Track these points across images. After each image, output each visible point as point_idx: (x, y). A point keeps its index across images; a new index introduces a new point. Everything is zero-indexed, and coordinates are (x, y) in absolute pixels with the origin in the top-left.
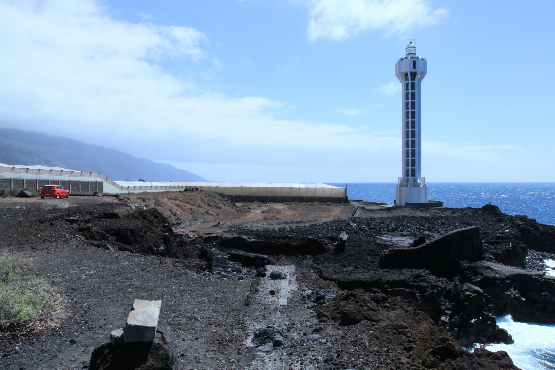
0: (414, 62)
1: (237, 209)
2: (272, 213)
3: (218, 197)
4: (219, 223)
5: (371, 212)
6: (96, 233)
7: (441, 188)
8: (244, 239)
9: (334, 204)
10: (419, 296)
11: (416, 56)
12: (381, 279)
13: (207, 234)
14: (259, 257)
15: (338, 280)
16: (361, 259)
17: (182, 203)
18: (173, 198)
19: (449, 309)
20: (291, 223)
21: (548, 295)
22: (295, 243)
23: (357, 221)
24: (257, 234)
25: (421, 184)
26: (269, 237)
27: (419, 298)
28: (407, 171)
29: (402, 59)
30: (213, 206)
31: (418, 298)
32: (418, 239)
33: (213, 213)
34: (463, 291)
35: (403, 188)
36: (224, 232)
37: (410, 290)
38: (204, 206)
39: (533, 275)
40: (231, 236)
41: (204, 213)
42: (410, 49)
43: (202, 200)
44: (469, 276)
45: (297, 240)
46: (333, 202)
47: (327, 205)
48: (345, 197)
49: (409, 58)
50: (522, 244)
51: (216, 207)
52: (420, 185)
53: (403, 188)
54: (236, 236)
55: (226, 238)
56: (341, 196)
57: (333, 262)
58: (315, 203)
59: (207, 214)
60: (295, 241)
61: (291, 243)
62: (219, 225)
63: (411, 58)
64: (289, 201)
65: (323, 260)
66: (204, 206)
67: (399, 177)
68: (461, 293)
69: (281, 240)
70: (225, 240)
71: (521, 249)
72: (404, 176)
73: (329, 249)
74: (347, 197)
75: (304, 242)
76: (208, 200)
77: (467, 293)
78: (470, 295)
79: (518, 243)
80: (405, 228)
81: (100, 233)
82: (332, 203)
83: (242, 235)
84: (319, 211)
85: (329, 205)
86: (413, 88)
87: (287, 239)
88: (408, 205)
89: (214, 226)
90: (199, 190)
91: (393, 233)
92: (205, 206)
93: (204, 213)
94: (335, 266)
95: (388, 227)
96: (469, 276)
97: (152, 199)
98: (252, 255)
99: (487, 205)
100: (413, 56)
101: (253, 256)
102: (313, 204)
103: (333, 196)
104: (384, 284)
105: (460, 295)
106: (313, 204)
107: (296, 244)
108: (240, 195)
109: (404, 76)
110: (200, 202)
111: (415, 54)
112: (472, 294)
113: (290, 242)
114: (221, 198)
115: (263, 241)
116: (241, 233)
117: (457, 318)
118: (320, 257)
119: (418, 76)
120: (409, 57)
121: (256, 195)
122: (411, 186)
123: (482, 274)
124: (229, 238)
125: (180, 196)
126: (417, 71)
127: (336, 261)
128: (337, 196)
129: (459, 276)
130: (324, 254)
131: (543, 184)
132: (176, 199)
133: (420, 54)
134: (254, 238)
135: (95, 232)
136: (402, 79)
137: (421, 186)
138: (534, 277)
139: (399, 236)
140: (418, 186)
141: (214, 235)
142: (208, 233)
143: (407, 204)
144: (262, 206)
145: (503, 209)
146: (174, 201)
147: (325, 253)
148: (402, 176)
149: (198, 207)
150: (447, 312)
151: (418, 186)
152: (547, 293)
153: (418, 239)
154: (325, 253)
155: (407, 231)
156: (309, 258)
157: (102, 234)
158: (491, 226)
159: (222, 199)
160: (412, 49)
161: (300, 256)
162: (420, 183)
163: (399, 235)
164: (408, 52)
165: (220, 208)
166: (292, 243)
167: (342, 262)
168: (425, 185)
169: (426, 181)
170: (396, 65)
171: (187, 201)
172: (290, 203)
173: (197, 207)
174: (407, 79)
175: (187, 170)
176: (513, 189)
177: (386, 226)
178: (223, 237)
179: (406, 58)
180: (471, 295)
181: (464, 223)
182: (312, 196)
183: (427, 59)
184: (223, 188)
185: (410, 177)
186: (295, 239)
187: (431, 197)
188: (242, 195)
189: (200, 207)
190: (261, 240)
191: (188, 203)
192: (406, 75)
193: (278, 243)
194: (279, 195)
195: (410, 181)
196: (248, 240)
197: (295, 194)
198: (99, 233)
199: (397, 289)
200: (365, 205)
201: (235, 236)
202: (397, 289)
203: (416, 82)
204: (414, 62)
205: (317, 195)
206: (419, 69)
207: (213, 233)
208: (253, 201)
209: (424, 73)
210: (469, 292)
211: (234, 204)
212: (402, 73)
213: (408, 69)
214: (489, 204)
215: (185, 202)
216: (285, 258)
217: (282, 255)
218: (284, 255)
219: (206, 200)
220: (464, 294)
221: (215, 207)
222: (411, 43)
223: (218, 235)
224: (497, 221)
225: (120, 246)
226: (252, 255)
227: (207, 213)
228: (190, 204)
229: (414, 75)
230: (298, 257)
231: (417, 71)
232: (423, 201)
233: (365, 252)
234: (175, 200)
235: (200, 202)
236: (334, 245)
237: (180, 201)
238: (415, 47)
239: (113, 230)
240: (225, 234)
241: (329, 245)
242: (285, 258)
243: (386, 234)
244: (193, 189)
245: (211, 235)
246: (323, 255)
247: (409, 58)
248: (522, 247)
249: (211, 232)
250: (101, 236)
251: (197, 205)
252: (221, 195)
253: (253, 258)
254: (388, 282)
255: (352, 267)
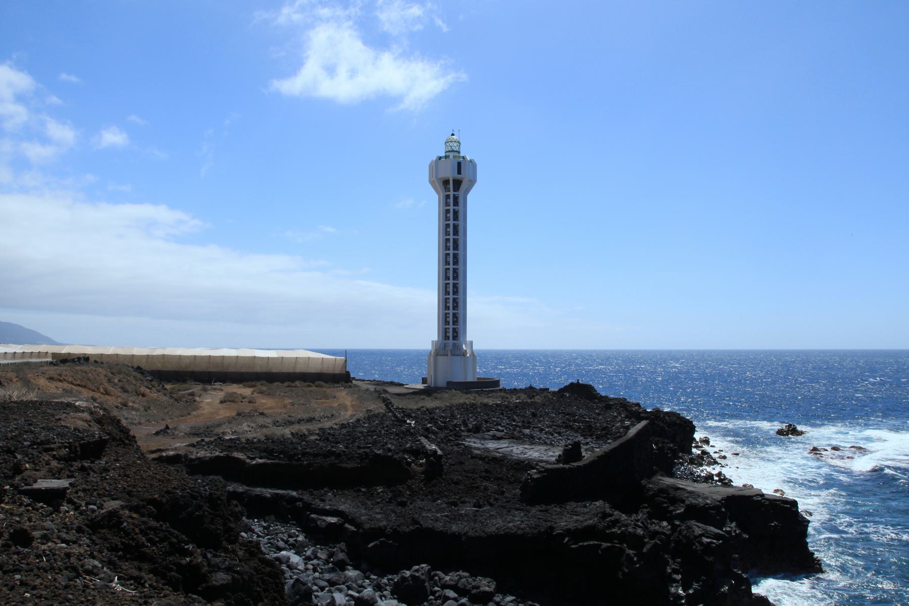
0: (459, 164)
1: (173, 397)
2: (240, 403)
3: (133, 373)
4: (167, 427)
5: (403, 397)
6: (141, 531)
7: (500, 357)
8: (238, 458)
9: (328, 385)
10: (634, 554)
11: (462, 155)
12: (552, 528)
13: (153, 452)
14: (282, 497)
15: (465, 534)
16: (477, 487)
17: (73, 386)
18: (56, 376)
19: (675, 571)
20: (299, 423)
21: (779, 526)
22: (350, 465)
23: (413, 415)
24: (268, 447)
25: (468, 351)
26: (295, 455)
27: (635, 559)
28: (446, 331)
29: (440, 158)
30: (132, 392)
31: (633, 558)
32: (570, 447)
33: (136, 406)
34: (696, 537)
35: (441, 359)
36: (189, 445)
37: (609, 545)
38: (116, 391)
39: (753, 496)
40: (209, 455)
41: (119, 405)
42: (451, 144)
43: (109, 381)
44: (665, 505)
45: (351, 457)
46: (326, 382)
47: (316, 386)
48: (344, 372)
49: (451, 157)
50: (670, 443)
51: (136, 393)
52: (467, 354)
53: (440, 359)
54: (222, 455)
55: (199, 459)
56: (337, 371)
57: (430, 497)
58: (297, 383)
59: (124, 408)
60: (349, 459)
61: (342, 465)
62: (169, 431)
63: (454, 157)
64: (252, 380)
65: (410, 495)
66: (116, 391)
67: (433, 342)
68: (695, 542)
69: (319, 460)
70: (196, 462)
71: (669, 452)
72: (441, 339)
73: (414, 472)
74: (348, 373)
75: (367, 461)
76: (119, 381)
77: (705, 540)
78: (711, 543)
79: (663, 443)
80: (492, 425)
81: (154, 529)
82: (324, 384)
83: (232, 452)
84: (319, 397)
85: (321, 387)
86: (456, 203)
87: (333, 458)
88: (452, 386)
89: (157, 433)
90: (92, 360)
91: (478, 435)
92: (116, 391)
93: (119, 405)
94: (437, 505)
95: (466, 425)
96: (665, 505)
97: (15, 380)
98: (268, 492)
99: (572, 384)
100: (457, 154)
101: (268, 495)
102: (293, 385)
103: (325, 371)
104: (561, 536)
105: (695, 545)
106: (293, 385)
107: (352, 466)
108: (160, 369)
109: (442, 184)
110: (106, 384)
111: (459, 152)
112: (715, 541)
113: (339, 463)
114: (139, 376)
115: (281, 462)
116: (230, 447)
117: (695, 585)
118: (402, 489)
119: (463, 187)
120: (451, 155)
121: (190, 370)
122: (453, 355)
123: (683, 501)
124: (206, 459)
125: (53, 371)
126: (463, 179)
127: (436, 496)
128: (330, 371)
129: (646, 508)
130: (407, 483)
131: (645, 351)
132: (61, 379)
133: (467, 152)
134: (261, 458)
135: (137, 530)
136: (438, 186)
137: (468, 355)
138: (755, 498)
139: (491, 440)
140: (464, 354)
141: (172, 453)
142: (154, 449)
143: (449, 383)
144: (209, 390)
145: (601, 389)
146: (59, 384)
147: (409, 481)
148: (437, 339)
149: (104, 394)
150: (675, 576)
151: (464, 355)
152: (776, 523)
153: (570, 447)
154: (409, 481)
155: (496, 430)
156: (382, 492)
157: (161, 535)
158: (600, 417)
159: (142, 378)
160: (455, 144)
161: (363, 490)
162: (466, 351)
163: (491, 438)
164: (450, 149)
165: (143, 395)
166: (344, 465)
167: (446, 496)
168: (472, 353)
169: (475, 348)
170: (431, 166)
171: (83, 384)
172: (253, 383)
173: (102, 393)
174: (446, 189)
175: (19, 324)
176: (607, 358)
177: (463, 422)
178: (194, 457)
179: (446, 157)
180: (714, 543)
181: (563, 413)
182: (291, 370)
183: (477, 161)
184: (125, 356)
185: (451, 341)
186: (349, 456)
187: (481, 372)
188: (163, 369)
189: (108, 394)
190: (277, 461)
191: (85, 387)
192: (446, 182)
193: (316, 465)
194: (231, 370)
195: (451, 347)
196: (248, 461)
197: (259, 368)
198: (151, 528)
199: (586, 544)
200: (381, 389)
201: (217, 453)
202: (586, 544)
203: (460, 193)
204: (459, 164)
205: (298, 370)
206: (465, 175)
207: (167, 450)
208: (184, 381)
209: (473, 182)
210: (707, 537)
211: (163, 386)
212: (440, 178)
213: (449, 173)
214: (576, 382)
215: (79, 385)
216: (335, 496)
217: (325, 489)
218: (331, 489)
219: (116, 381)
220: (701, 543)
221: (134, 393)
222: (453, 135)
223: (180, 452)
224: (605, 409)
225: (237, 572)
226: (268, 492)
227: (125, 405)
228: (90, 389)
229: (457, 184)
230: (359, 491)
231: (463, 179)
232: (470, 379)
233: (476, 473)
234: (60, 381)
235: (106, 384)
236: (421, 465)
237: (68, 382)
238: (459, 142)
239: (152, 502)
240: (192, 449)
241: (413, 464)
242: (335, 496)
243: (468, 436)
244: (79, 359)
245: (164, 454)
246: (407, 485)
247: (451, 157)
248: (670, 448)
249: (162, 448)
250: (162, 540)
251: (102, 390)
252: (139, 369)
253: (270, 498)
254: (568, 532)
255: (468, 504)
